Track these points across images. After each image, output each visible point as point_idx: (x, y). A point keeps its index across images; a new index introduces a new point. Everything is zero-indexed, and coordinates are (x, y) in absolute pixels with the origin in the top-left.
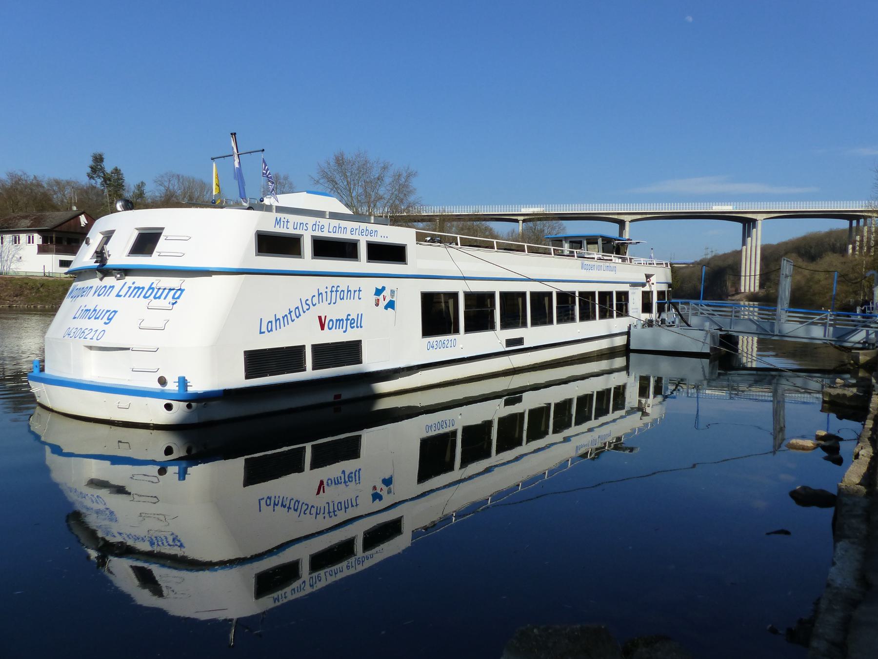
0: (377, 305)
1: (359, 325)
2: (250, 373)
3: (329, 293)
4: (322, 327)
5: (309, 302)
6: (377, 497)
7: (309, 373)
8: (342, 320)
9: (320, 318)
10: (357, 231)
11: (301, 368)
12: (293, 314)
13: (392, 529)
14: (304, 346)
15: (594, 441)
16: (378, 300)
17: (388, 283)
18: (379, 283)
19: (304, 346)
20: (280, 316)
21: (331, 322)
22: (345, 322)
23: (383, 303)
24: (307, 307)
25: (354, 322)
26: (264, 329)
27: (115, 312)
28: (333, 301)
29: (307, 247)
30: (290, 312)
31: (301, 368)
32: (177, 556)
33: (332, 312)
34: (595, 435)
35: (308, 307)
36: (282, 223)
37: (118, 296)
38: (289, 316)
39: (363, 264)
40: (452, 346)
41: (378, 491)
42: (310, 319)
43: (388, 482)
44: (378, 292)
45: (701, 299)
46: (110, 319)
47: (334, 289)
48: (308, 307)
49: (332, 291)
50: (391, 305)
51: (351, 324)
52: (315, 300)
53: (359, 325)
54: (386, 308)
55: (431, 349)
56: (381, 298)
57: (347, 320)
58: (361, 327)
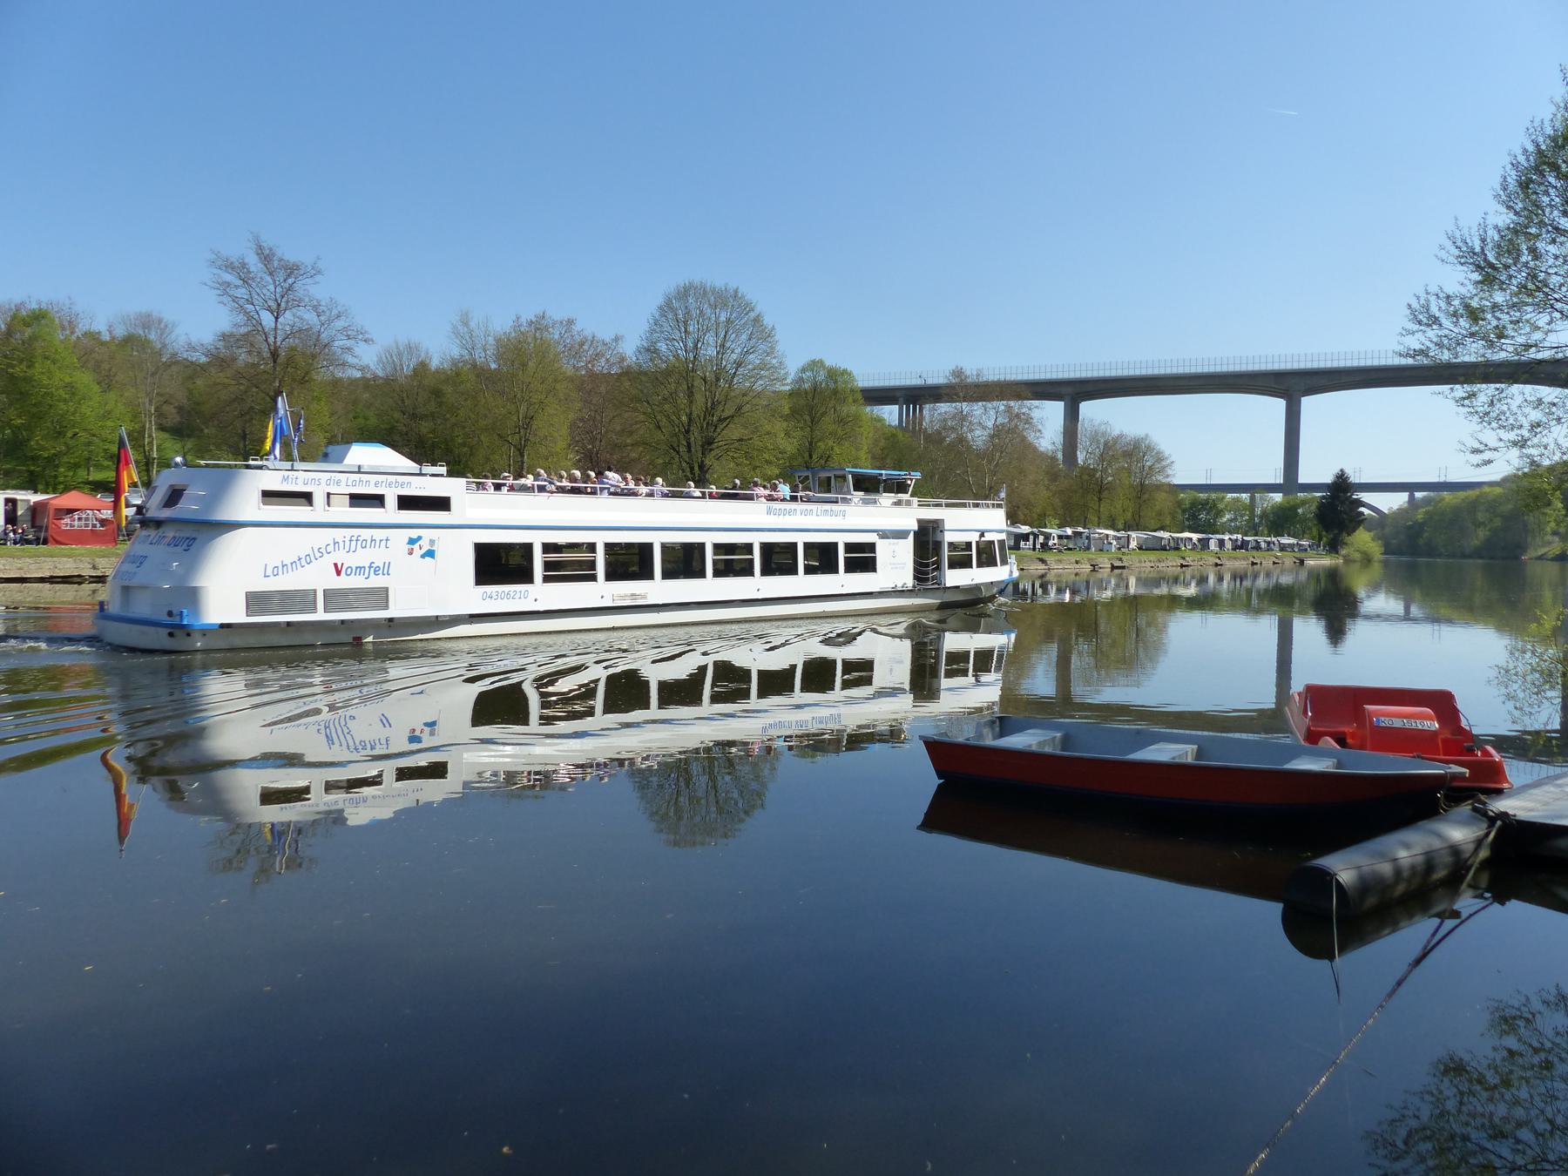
0: (411, 553)
1: (385, 572)
2: (250, 610)
3: (347, 543)
4: (338, 573)
5: (323, 550)
6: (414, 739)
7: (320, 615)
8: (364, 567)
9: (336, 565)
10: (384, 484)
11: (314, 610)
12: (303, 561)
13: (437, 771)
14: (978, 567)
15: (799, 723)
16: (412, 549)
17: (426, 534)
18: (414, 533)
19: (978, 567)
20: (287, 562)
21: (348, 573)
22: (367, 569)
23: (418, 552)
24: (318, 555)
25: (385, 569)
26: (269, 572)
27: (146, 557)
28: (353, 548)
29: (391, 502)
30: (300, 559)
31: (314, 610)
32: (1386, 587)
33: (349, 560)
34: (804, 715)
35: (321, 555)
36: (290, 480)
37: (151, 544)
38: (298, 562)
39: (391, 513)
40: (522, 597)
41: (417, 733)
42: (327, 563)
43: (432, 724)
44: (412, 541)
45: (847, 555)
46: (141, 563)
47: (354, 539)
48: (321, 555)
49: (351, 541)
50: (430, 554)
51: (375, 571)
52: (330, 548)
53: (385, 572)
54: (423, 556)
55: (488, 599)
56: (416, 547)
57: (370, 567)
58: (388, 574)
